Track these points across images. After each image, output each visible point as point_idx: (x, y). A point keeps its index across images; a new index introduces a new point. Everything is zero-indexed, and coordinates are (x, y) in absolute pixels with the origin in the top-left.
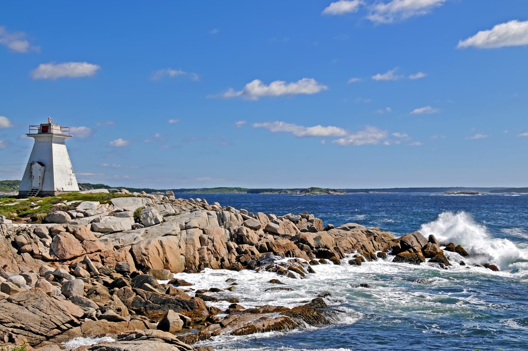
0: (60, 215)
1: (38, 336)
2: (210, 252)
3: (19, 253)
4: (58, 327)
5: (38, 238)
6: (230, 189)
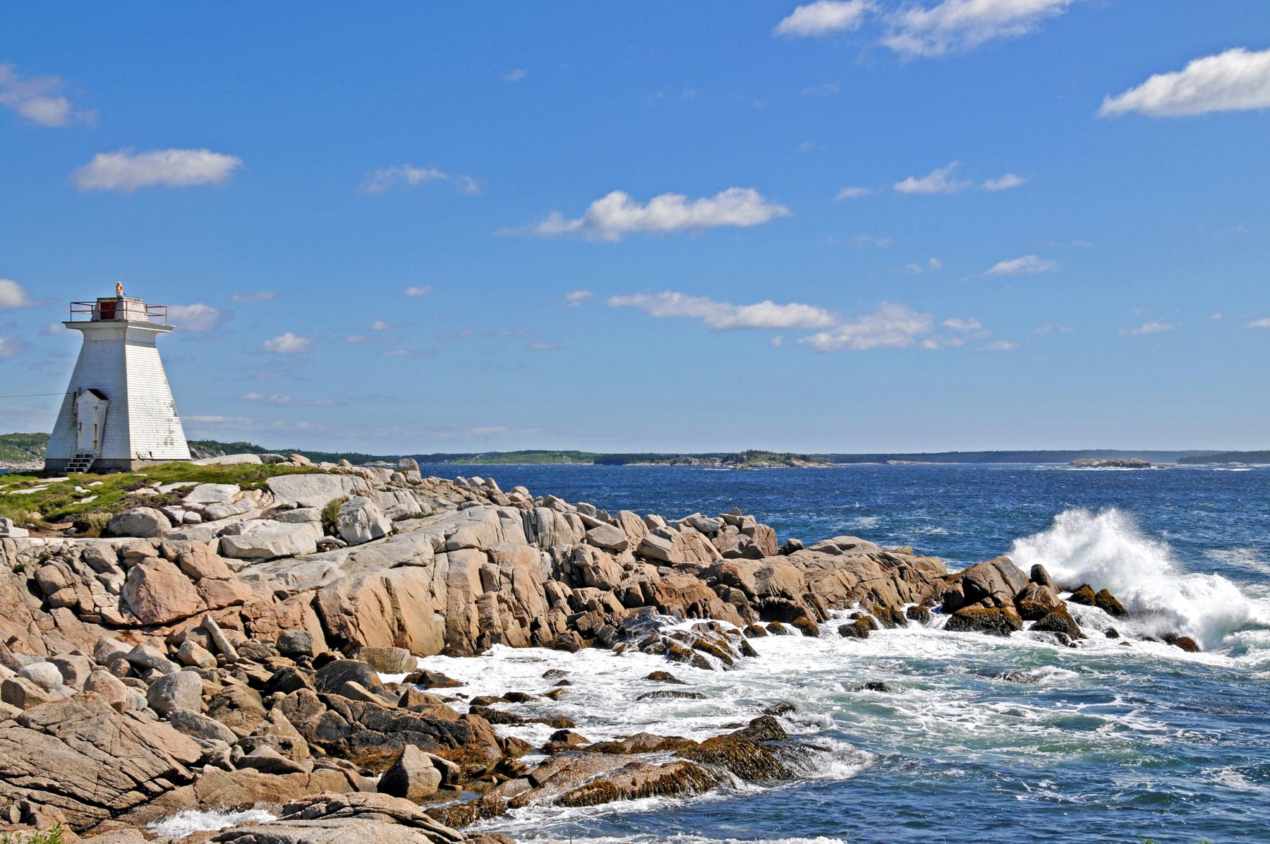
0: (144, 516)
1: (92, 809)
3: (46, 608)
4: (140, 787)
5: (91, 573)
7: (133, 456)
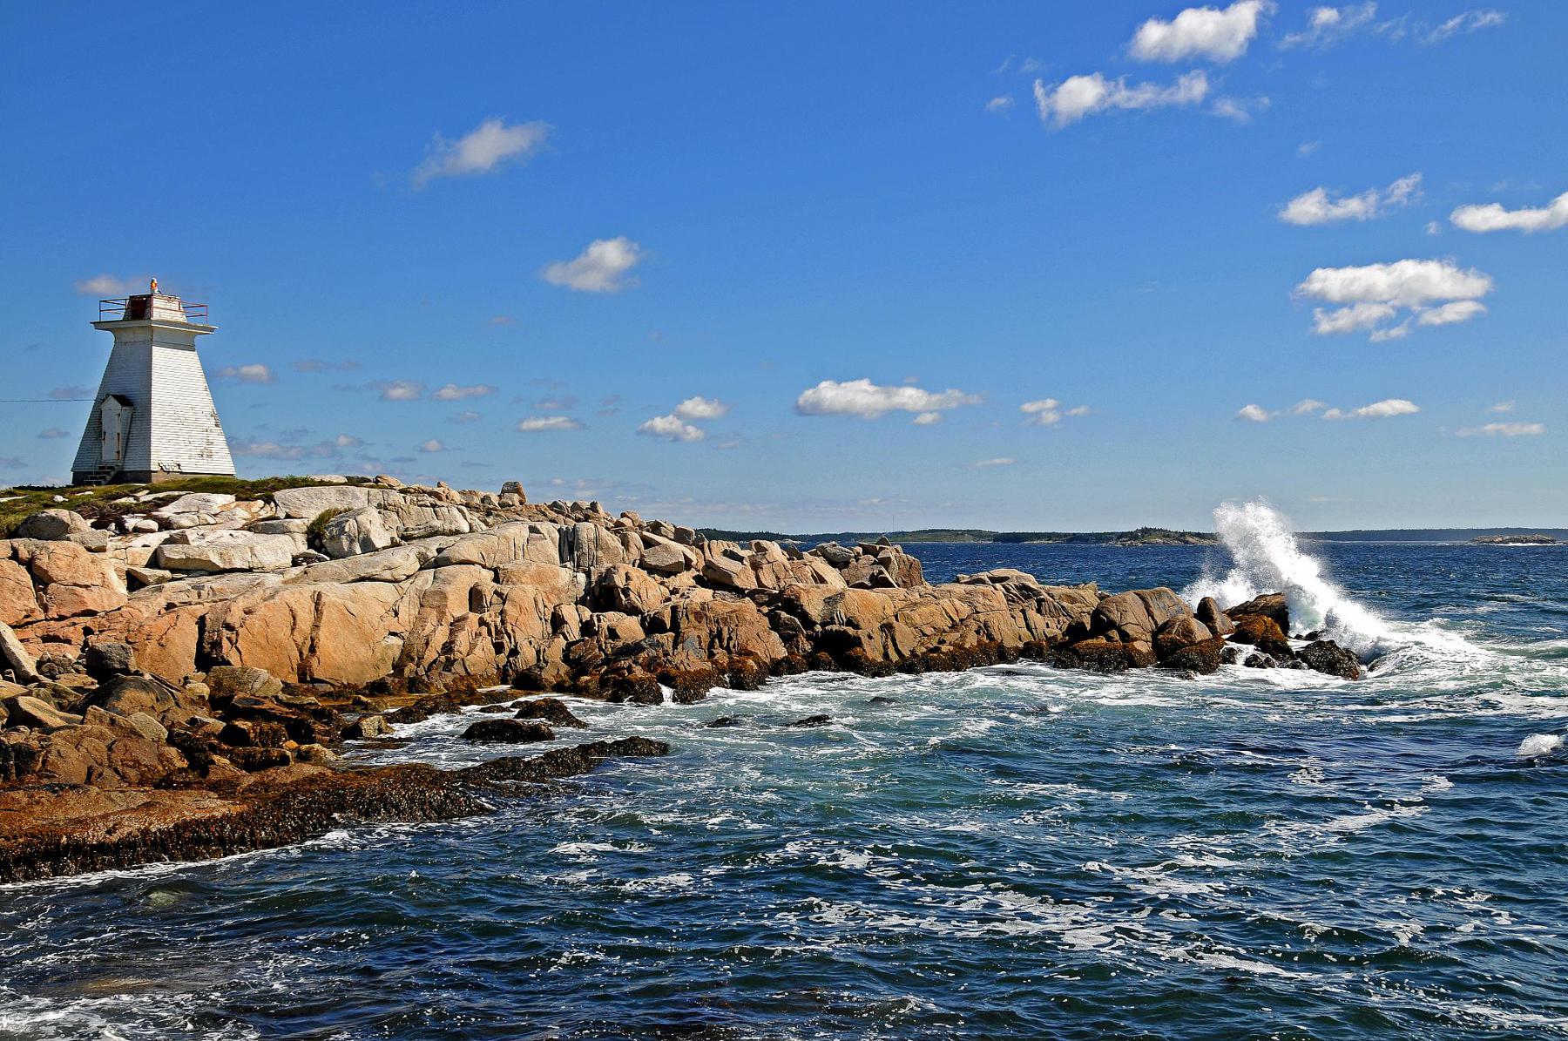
0: (53, 519)
2: (485, 629)
6: (956, 533)
7: (154, 467)
